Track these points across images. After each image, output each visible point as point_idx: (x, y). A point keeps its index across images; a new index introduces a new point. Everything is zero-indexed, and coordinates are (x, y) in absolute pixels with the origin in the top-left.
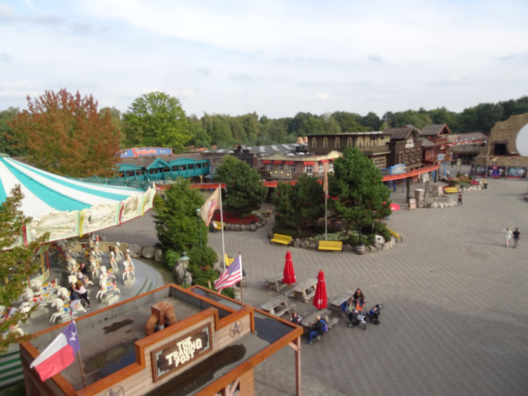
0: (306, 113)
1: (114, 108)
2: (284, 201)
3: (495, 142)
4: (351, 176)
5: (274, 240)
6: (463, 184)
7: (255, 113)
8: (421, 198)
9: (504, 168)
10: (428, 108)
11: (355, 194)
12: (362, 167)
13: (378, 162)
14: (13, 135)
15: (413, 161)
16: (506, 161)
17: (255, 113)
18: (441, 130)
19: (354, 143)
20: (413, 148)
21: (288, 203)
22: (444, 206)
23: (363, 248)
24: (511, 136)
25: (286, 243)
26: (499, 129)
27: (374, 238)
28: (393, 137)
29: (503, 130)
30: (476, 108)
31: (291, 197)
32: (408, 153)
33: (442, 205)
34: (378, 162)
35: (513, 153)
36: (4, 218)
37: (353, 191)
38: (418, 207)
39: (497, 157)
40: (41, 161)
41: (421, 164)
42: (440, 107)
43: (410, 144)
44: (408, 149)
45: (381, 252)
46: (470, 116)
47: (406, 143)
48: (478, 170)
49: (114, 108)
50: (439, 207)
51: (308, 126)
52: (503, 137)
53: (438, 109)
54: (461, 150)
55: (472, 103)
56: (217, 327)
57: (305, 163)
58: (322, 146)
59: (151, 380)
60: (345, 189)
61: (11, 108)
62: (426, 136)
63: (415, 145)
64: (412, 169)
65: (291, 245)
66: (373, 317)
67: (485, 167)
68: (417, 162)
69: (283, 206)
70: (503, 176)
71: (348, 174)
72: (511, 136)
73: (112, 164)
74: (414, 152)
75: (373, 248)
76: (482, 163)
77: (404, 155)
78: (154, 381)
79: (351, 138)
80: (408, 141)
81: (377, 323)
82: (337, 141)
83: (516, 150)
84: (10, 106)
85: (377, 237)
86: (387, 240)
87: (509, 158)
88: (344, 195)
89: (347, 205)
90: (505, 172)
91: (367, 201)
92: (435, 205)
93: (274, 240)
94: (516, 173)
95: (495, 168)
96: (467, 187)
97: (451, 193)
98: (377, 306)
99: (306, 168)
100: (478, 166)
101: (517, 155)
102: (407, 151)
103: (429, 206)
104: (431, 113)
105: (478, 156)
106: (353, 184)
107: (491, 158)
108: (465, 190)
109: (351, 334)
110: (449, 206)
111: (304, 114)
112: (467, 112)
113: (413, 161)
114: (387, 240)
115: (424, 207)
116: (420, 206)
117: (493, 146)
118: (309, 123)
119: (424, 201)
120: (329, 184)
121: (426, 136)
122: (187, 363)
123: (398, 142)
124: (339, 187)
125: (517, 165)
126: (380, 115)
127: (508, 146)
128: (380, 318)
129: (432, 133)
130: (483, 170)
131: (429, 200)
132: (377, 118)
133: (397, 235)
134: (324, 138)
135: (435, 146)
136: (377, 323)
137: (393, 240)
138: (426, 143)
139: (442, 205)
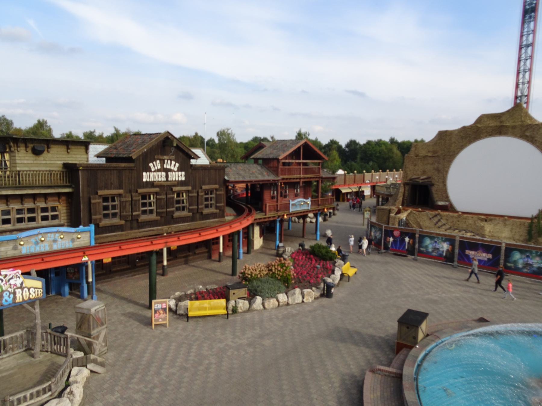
3: (411, 180)
7: (196, 134)
9: (412, 236)
13: (27, 216)
16: (424, 220)
17: (196, 134)
24: (438, 170)
26: (417, 156)
29: (425, 157)
34: (27, 216)
35: (441, 203)
36: (324, 244)
39: (410, 210)
40: (538, 145)
52: (424, 172)
67: (381, 230)
70: (411, 251)
72: (438, 170)
73: (531, 253)
83: (447, 198)
84: (88, 130)
87: (431, 213)
90: (414, 243)
94: (435, 249)
95: (396, 233)
101: (449, 208)
107: (399, 212)
117: (407, 188)
125: (442, 232)
127: (434, 189)
130: (378, 234)
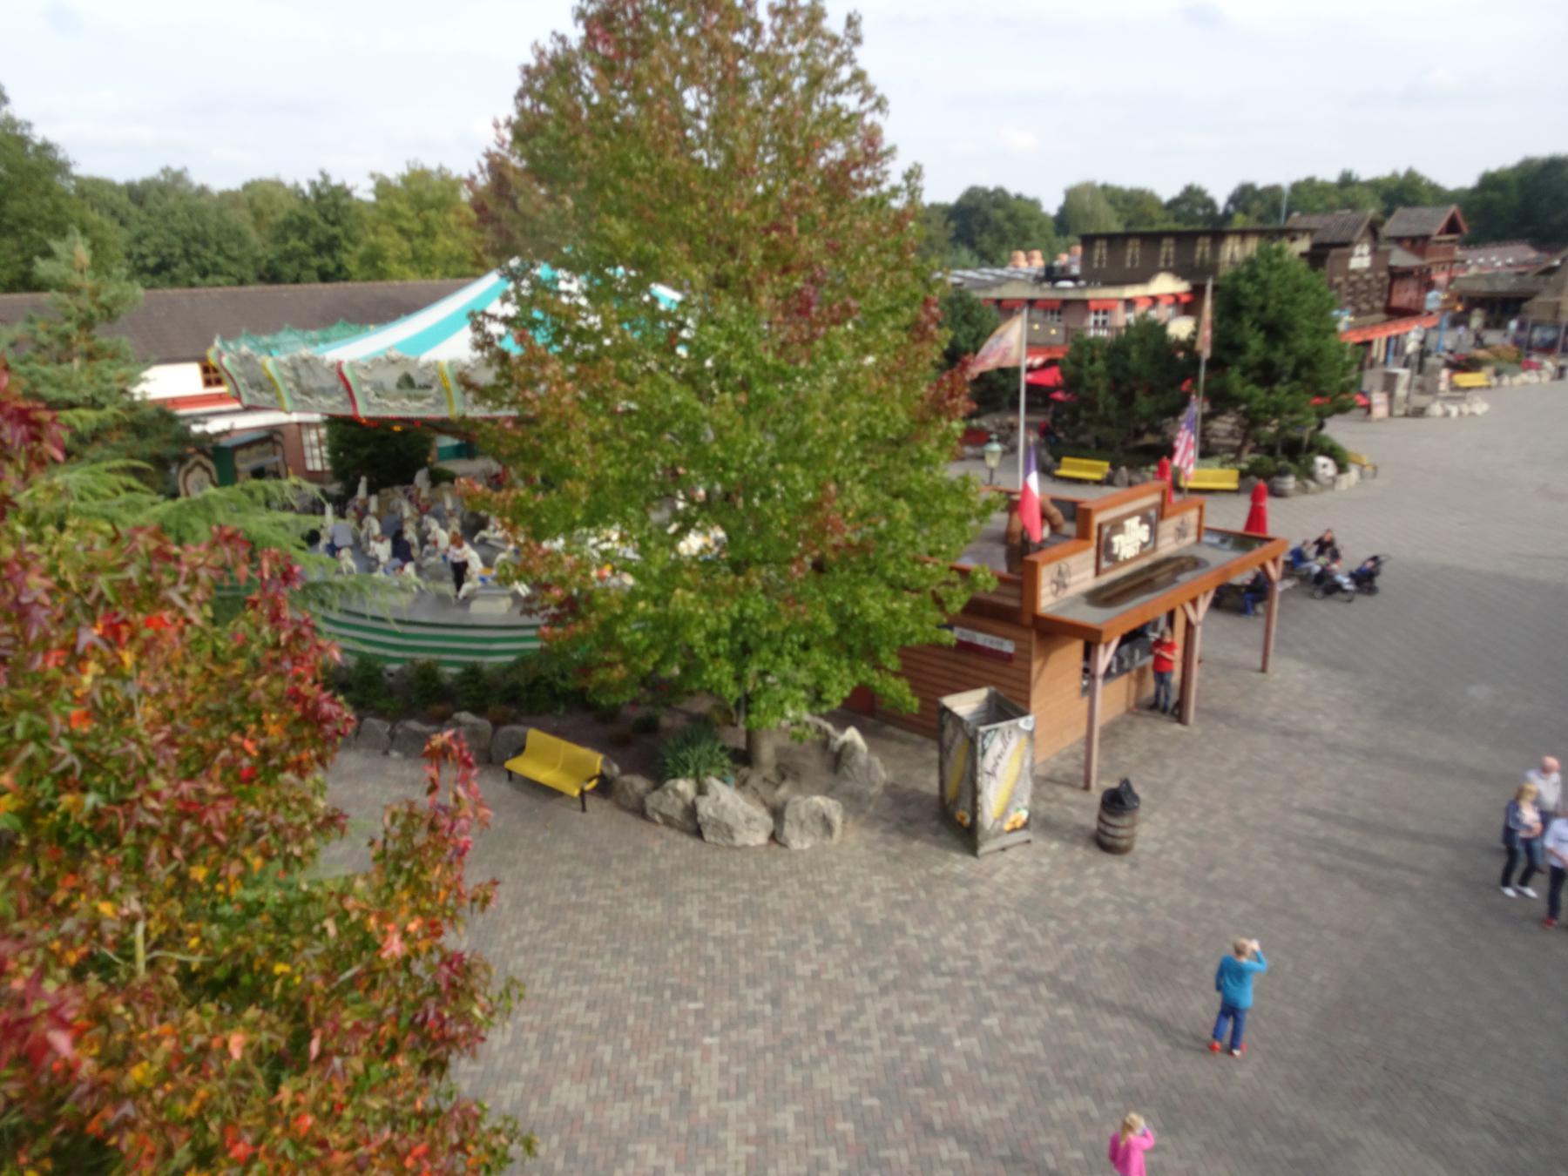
0: (991, 188)
1: (441, 169)
2: (1093, 376)
4: (1271, 312)
5: (522, 766)
6: (1502, 365)
8: (1401, 391)
10: (1367, 171)
11: (1278, 356)
12: (1297, 290)
14: (206, 245)
15: (1364, 307)
18: (1443, 222)
19: (1215, 252)
20: (1369, 270)
21: (1102, 384)
22: (1460, 414)
23: (1290, 482)
25: (1098, 476)
27: (1312, 462)
28: (1318, 237)
30: (1514, 170)
31: (1110, 368)
32: (1353, 284)
33: (1454, 410)
37: (1275, 348)
38: (1391, 414)
41: (1382, 316)
42: (1402, 172)
43: (1361, 260)
44: (1354, 272)
45: (1328, 495)
46: (1497, 195)
47: (1351, 255)
48: (1537, 335)
49: (441, 169)
50: (1447, 414)
51: (1008, 226)
53: (1395, 175)
54: (1482, 287)
55: (1504, 156)
56: (1168, 510)
57: (1093, 305)
58: (1123, 262)
59: (1092, 571)
60: (1256, 343)
61: (166, 171)
62: (1399, 240)
63: (1374, 262)
64: (450, 863)
65: (1109, 481)
66: (1365, 579)
67: (1557, 327)
68: (1373, 311)
69: (1089, 389)
71: (1263, 308)
74: (1368, 282)
75: (1312, 484)
76: (1548, 317)
77: (1344, 287)
78: (1098, 572)
79: (1207, 240)
80: (1358, 250)
81: (1372, 590)
82: (1168, 248)
84: (163, 165)
85: (1321, 460)
86: (1342, 468)
88: (1251, 357)
89: (1256, 381)
91: (1305, 373)
92: (1437, 409)
93: (1062, 472)
96: (1513, 374)
97: (1469, 389)
98: (1375, 559)
99: (1092, 318)
100: (1535, 325)
102: (1353, 278)
103: (1420, 412)
104: (1374, 185)
105: (1539, 299)
106: (1275, 331)
108: (1506, 380)
109: (1323, 608)
110: (1472, 414)
111: (986, 193)
112: (1490, 182)
113: (1364, 307)
114: (1342, 468)
115: (1406, 415)
116: (1397, 412)
118: (1011, 218)
119: (1407, 400)
120: (1214, 331)
121: (1399, 240)
122: (1132, 560)
123: (1334, 252)
124: (1237, 340)
126: (1220, 195)
128: (1379, 581)
129: (1416, 230)
130: (1550, 335)
131: (1419, 400)
132: (1210, 204)
133: (1365, 460)
134: (1131, 242)
135: (1420, 268)
136: (1372, 590)
137: (1354, 473)
138: (1401, 258)
139: (1454, 410)
